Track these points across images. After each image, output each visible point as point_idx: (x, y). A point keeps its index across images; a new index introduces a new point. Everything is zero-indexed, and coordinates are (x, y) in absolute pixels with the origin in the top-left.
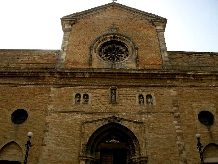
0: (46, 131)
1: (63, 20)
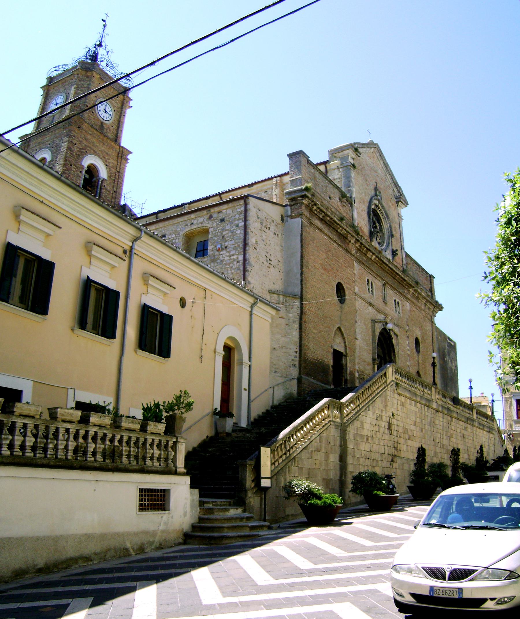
0: (356, 322)
1: (290, 156)
